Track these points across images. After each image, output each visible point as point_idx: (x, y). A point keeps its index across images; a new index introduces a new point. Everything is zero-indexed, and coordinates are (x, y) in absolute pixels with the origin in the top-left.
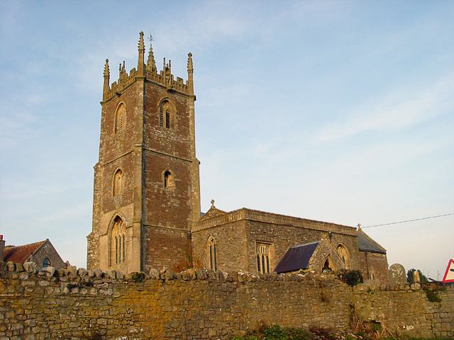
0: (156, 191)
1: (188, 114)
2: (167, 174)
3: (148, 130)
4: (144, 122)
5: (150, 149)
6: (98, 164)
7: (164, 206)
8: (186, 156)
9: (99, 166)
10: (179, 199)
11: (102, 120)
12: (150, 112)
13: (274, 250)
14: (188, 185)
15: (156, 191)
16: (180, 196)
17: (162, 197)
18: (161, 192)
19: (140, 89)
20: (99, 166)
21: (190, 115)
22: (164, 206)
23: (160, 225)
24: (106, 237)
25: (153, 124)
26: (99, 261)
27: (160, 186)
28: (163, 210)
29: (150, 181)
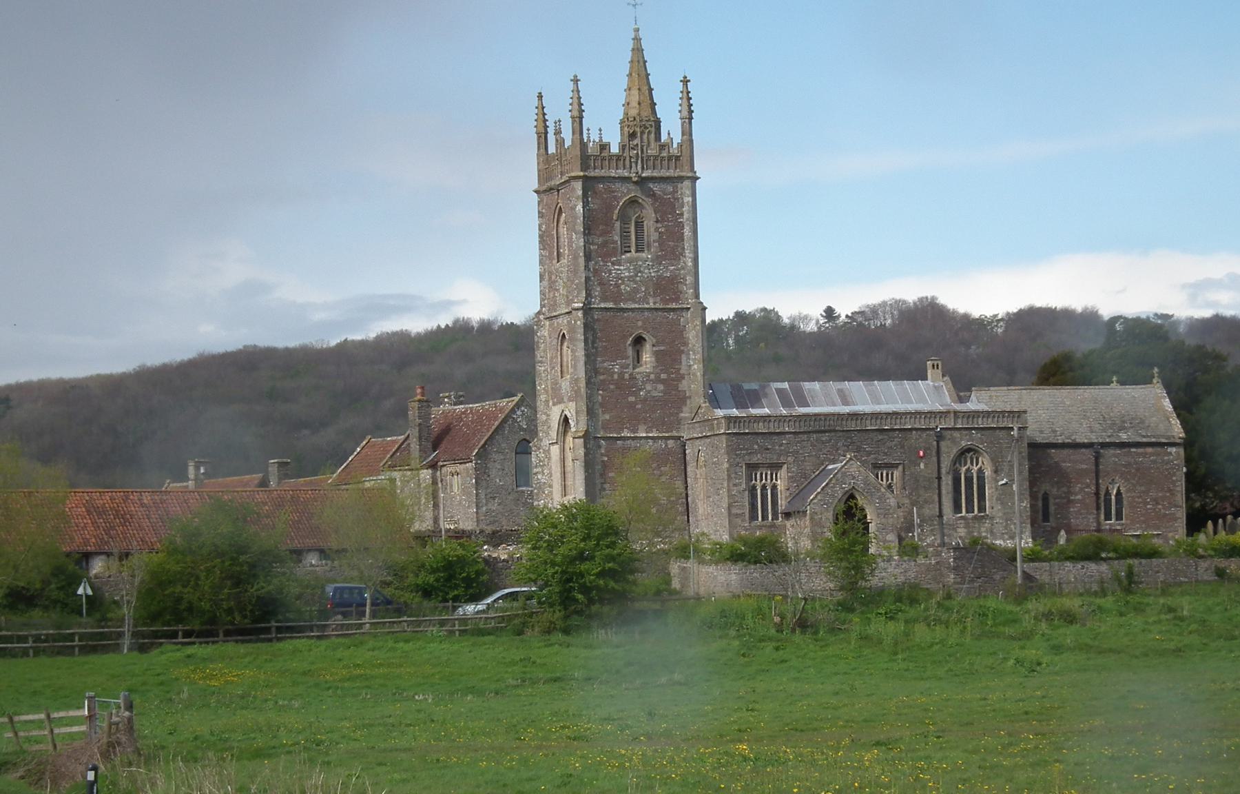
0: (616, 376)
1: (682, 214)
2: (639, 341)
3: (596, 271)
4: (588, 257)
5: (602, 305)
6: (539, 313)
7: (631, 399)
8: (677, 300)
9: (542, 317)
10: (663, 382)
11: (540, 226)
12: (601, 235)
13: (47, 751)
14: (683, 352)
15: (616, 376)
16: (663, 376)
17: (627, 385)
18: (627, 376)
19: (577, 198)
20: (542, 317)
21: (686, 216)
22: (631, 399)
23: (626, 433)
24: (556, 446)
25: (606, 256)
26: (551, 486)
27: (623, 367)
28: (632, 406)
29: (604, 362)
